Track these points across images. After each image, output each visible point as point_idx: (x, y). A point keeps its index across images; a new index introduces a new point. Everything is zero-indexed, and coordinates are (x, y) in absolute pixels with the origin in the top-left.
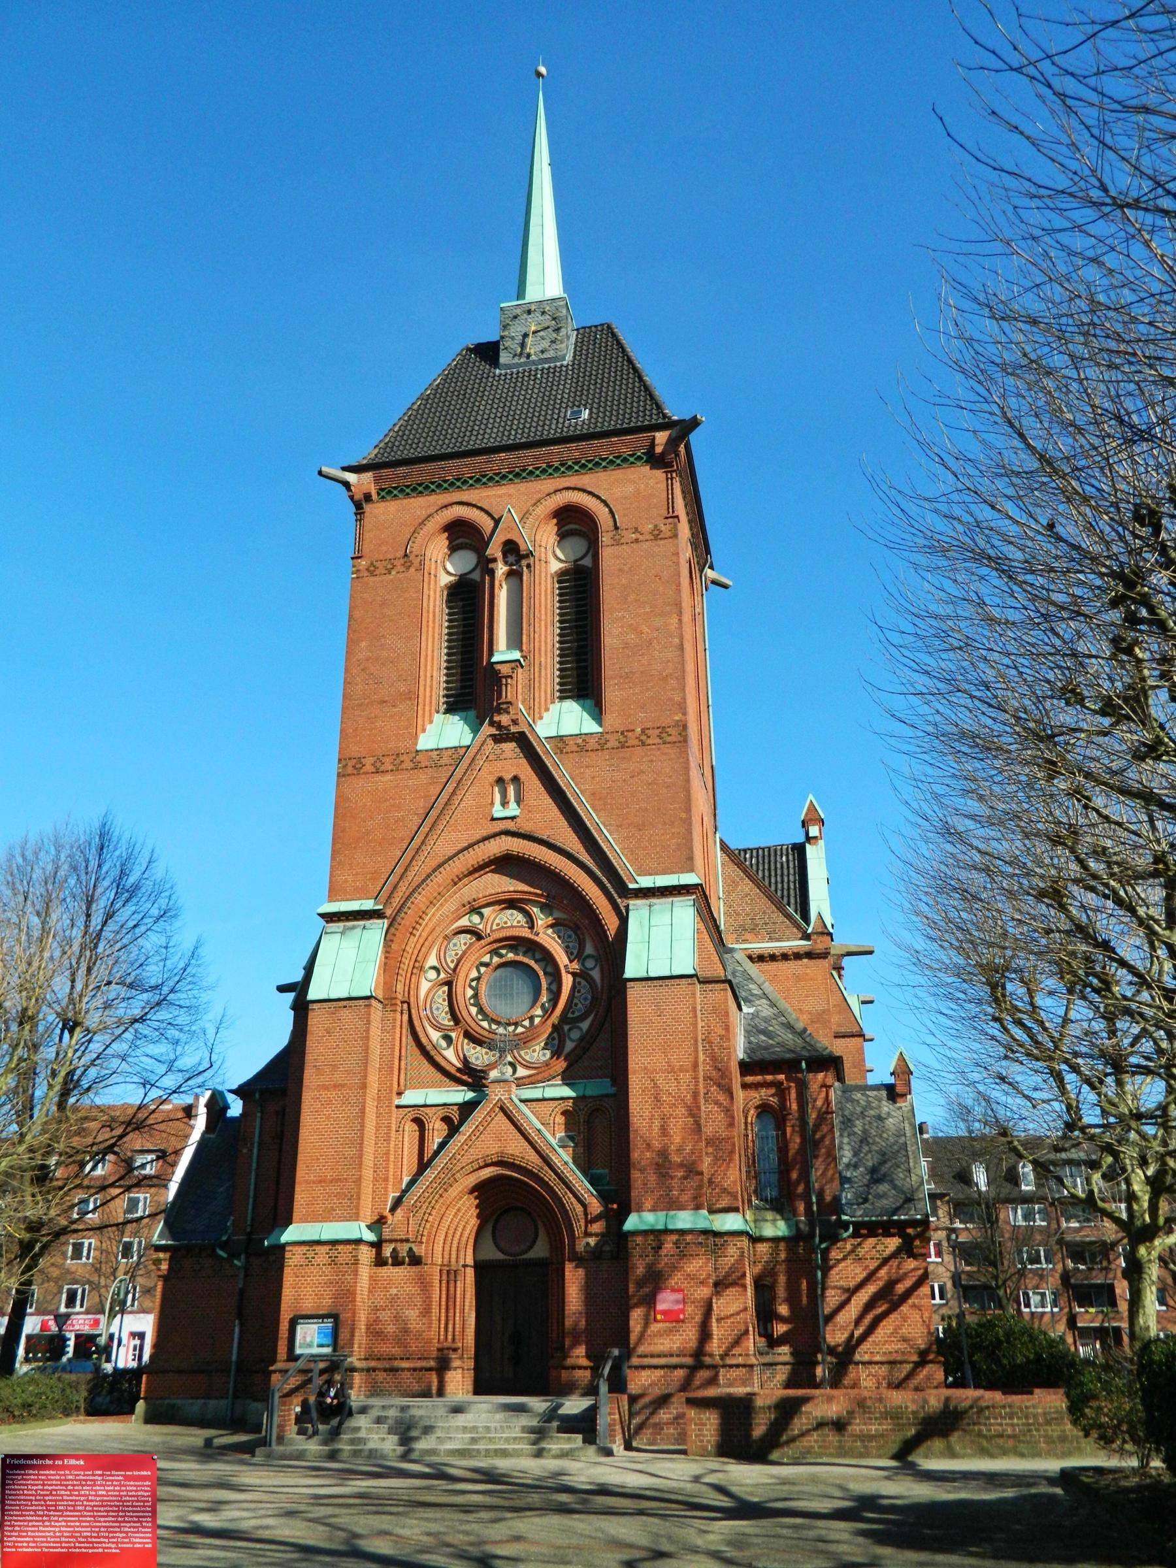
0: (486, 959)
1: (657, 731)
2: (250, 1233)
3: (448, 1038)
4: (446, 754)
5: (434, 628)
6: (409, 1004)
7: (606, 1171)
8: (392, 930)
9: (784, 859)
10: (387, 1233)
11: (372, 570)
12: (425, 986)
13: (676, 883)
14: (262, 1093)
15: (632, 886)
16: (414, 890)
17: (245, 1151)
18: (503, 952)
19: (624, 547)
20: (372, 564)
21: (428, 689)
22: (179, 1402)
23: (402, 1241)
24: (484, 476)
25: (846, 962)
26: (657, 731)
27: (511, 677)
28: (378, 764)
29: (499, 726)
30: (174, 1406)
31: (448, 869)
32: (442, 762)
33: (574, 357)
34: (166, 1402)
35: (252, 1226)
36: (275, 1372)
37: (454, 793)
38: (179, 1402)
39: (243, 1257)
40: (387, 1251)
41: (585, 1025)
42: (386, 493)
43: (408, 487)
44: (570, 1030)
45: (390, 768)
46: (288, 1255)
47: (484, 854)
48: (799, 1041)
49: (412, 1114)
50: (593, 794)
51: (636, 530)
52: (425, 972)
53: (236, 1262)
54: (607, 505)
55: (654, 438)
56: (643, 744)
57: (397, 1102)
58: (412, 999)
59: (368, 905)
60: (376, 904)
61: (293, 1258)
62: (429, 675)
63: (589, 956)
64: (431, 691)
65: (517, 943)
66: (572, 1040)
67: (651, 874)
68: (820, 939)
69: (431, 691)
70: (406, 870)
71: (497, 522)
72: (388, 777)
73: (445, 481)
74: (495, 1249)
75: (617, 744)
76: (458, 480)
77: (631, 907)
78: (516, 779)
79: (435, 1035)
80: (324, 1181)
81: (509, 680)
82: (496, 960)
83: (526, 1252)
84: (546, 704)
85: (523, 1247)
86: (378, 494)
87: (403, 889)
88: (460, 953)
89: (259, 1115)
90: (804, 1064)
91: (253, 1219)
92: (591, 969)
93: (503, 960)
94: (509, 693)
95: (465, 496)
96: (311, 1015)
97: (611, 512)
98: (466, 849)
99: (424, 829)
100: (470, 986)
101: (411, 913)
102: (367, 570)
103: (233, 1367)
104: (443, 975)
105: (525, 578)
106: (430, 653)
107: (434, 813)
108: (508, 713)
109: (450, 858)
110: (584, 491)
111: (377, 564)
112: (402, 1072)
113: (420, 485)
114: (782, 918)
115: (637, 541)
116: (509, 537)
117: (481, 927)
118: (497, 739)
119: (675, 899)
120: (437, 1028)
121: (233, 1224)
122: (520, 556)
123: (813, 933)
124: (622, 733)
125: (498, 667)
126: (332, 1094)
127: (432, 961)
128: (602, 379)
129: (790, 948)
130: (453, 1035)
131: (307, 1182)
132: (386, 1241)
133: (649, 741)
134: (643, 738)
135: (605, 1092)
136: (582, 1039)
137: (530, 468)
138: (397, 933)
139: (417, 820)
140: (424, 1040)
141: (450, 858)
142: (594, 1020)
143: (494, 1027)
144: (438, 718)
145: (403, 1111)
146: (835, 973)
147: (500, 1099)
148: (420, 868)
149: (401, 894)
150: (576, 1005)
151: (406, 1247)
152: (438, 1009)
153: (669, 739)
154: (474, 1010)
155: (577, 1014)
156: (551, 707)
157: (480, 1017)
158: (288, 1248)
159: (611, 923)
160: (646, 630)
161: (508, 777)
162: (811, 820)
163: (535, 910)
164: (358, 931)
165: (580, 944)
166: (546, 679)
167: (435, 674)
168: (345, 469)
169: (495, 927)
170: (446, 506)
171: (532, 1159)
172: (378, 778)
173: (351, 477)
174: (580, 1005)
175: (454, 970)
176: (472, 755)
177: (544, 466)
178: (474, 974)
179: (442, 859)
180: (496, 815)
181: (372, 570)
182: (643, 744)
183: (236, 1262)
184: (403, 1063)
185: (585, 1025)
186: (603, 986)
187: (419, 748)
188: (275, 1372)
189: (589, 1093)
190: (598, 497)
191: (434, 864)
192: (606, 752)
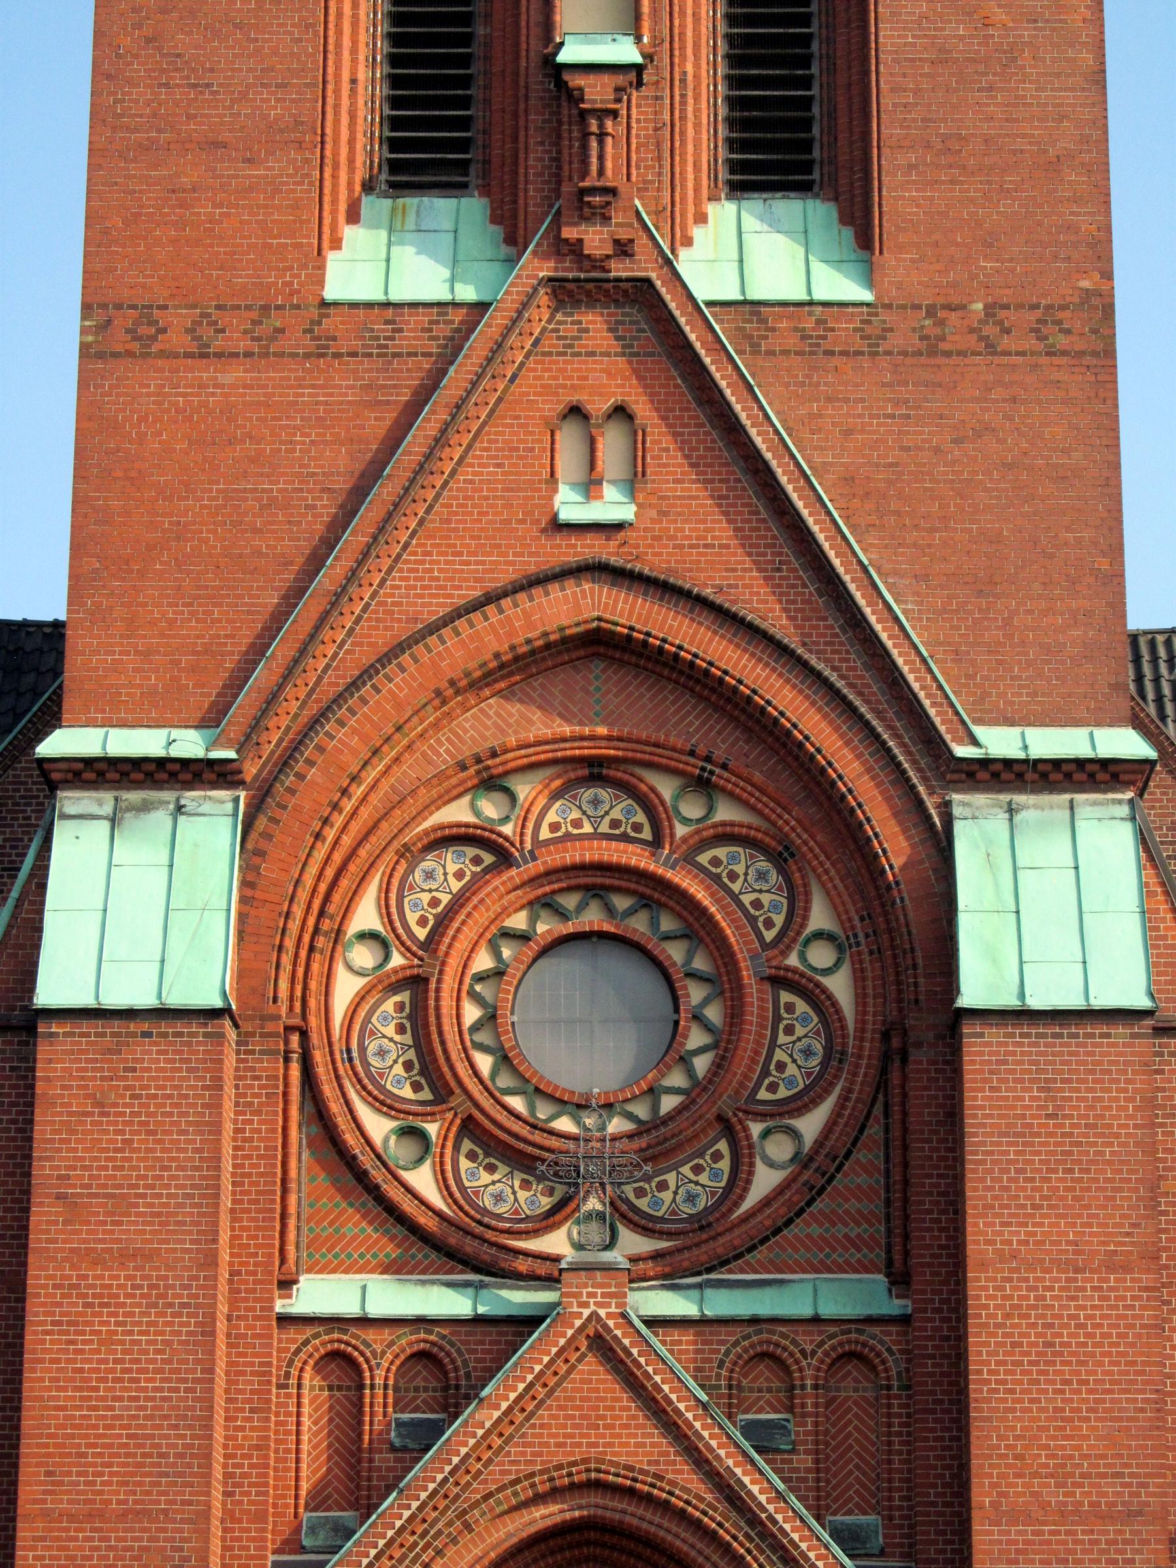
0: (519, 921)
1: (1032, 317)
6: (304, 1034)
7: (871, 1518)
8: (261, 823)
12: (346, 988)
15: (962, 751)
18: (570, 901)
26: (1032, 317)
27: (615, 114)
28: (206, 332)
29: (575, 249)
31: (425, 658)
32: (402, 343)
37: (441, 440)
41: (810, 1125)
44: (766, 1134)
45: (242, 346)
47: (530, 626)
49: (323, 1341)
52: (348, 946)
56: (991, 348)
57: (280, 1306)
58: (314, 1022)
60: (213, 744)
62: (346, 76)
63: (819, 935)
66: (771, 1164)
67: (1010, 722)
72: (232, 375)
77: (957, 811)
78: (621, 412)
80: (101, 1515)
81: (609, 124)
82: (544, 927)
84: (697, 203)
88: (445, 899)
92: (827, 972)
93: (569, 928)
96: (43, 1050)
98: (476, 606)
99: (354, 538)
100: (473, 995)
104: (397, 960)
107: (384, 492)
108: (606, 219)
109: (433, 629)
112: (292, 1222)
117: (507, 829)
119: (1080, 797)
120: (386, 1105)
124: (931, 312)
125: (576, 81)
130: (432, 1129)
131: (46, 1514)
133: (1005, 342)
134: (990, 330)
135: (874, 1311)
136: (801, 1161)
138: (276, 831)
139: (327, 508)
140: (351, 1139)
141: (433, 629)
142: (836, 1114)
143: (543, 1111)
144: (723, 213)
145: (298, 1335)
147: (594, 1315)
149: (285, 722)
152: (382, 1053)
153: (1062, 341)
154: (485, 1063)
156: (711, 209)
160: (1000, 15)
163: (666, 788)
164: (160, 819)
166: (698, 126)
167: (361, 76)
169: (545, 834)
172: (207, 373)
176: (494, 332)
178: (483, 962)
179: (401, 631)
182: (991, 348)
184: (293, 1199)
185: (810, 1125)
186: (861, 1022)
187: (331, 293)
189: (828, 1309)
191: (382, 640)
192: (884, 362)
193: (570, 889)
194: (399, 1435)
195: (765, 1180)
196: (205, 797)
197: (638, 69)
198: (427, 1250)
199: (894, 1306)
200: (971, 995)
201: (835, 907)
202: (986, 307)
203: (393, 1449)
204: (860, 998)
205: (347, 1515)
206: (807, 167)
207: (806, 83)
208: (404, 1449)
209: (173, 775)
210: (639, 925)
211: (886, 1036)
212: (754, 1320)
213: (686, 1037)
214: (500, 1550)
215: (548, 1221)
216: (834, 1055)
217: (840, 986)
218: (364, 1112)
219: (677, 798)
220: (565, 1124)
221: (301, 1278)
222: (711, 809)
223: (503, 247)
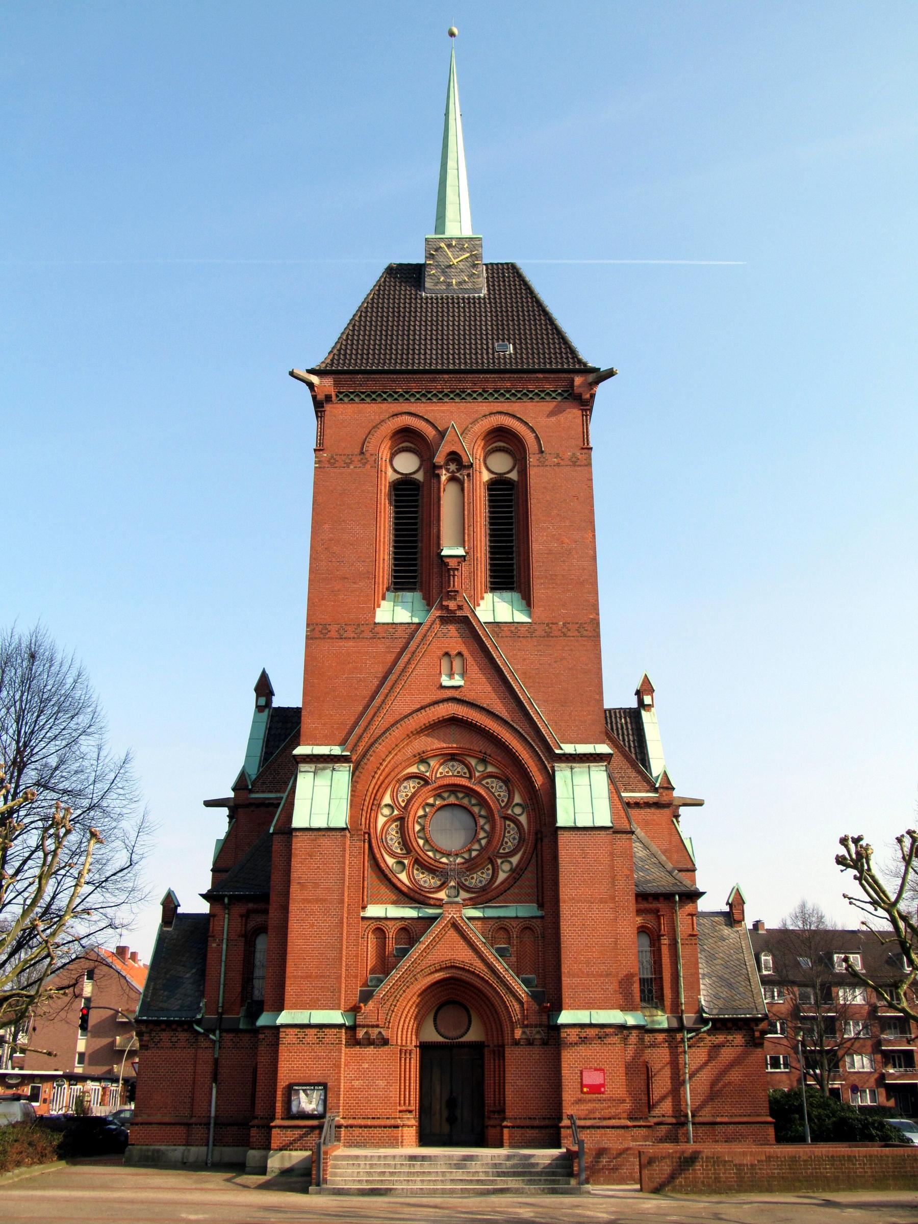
0: (431, 801)
2: (222, 1014)
3: (400, 863)
4: (400, 628)
5: (385, 518)
6: (369, 835)
8: (357, 773)
9: (623, 720)
10: (360, 1020)
11: (332, 462)
12: (381, 820)
13: (593, 751)
14: (230, 897)
16: (375, 741)
17: (214, 945)
19: (547, 468)
20: (332, 457)
21: (381, 570)
22: (163, 1148)
23: (373, 1026)
24: (430, 392)
25: (682, 810)
27: (457, 569)
28: (342, 632)
30: (158, 1151)
32: (397, 635)
33: (489, 290)
34: (152, 1147)
35: (222, 1007)
36: (275, 1127)
37: (408, 663)
38: (163, 1148)
39: (218, 1032)
40: (361, 1033)
41: (515, 860)
42: (343, 396)
43: (363, 393)
44: (502, 863)
45: (352, 635)
46: (282, 1035)
47: (434, 716)
48: (670, 879)
49: (374, 925)
50: (525, 673)
51: (557, 456)
52: (382, 809)
53: (212, 1036)
54: (533, 430)
55: (573, 381)
57: (362, 914)
58: (372, 831)
59: (337, 750)
61: (287, 1038)
62: (382, 558)
63: (517, 804)
64: (383, 571)
65: (453, 789)
66: (504, 871)
68: (665, 792)
69: (383, 571)
70: (369, 723)
71: (442, 434)
73: (396, 393)
74: (436, 1033)
75: (543, 634)
76: (407, 393)
78: (460, 654)
79: (390, 861)
80: (310, 977)
83: (462, 1036)
84: (481, 593)
85: (459, 1033)
86: (337, 396)
87: (366, 740)
88: (410, 794)
89: (227, 916)
90: (677, 897)
91: (223, 1003)
92: (519, 815)
93: (445, 803)
94: (456, 583)
95: (413, 408)
96: (294, 840)
97: (537, 437)
99: (384, 690)
101: (372, 759)
102: (329, 461)
103: (212, 1121)
104: (396, 812)
105: (466, 485)
106: (382, 540)
107: (392, 677)
108: (455, 599)
109: (406, 717)
110: (514, 416)
111: (337, 458)
113: (374, 393)
114: (634, 774)
115: (558, 464)
116: (453, 448)
117: (427, 774)
118: (444, 620)
120: (393, 855)
121: (206, 1005)
122: (461, 466)
123: (659, 787)
124: (548, 625)
126: (316, 907)
127: (387, 800)
128: (518, 316)
129: (642, 798)
130: (406, 862)
131: (295, 977)
132: (360, 1026)
135: (534, 915)
136: (512, 871)
137: (469, 391)
138: (362, 776)
140: (382, 865)
141: (406, 717)
146: (674, 820)
148: (380, 723)
149: (364, 744)
150: (506, 843)
151: (376, 1030)
152: (392, 839)
153: (585, 633)
154: (421, 842)
155: (507, 850)
156: (485, 595)
157: (427, 847)
158: (281, 1030)
159: (538, 780)
161: (453, 653)
162: (645, 690)
163: (473, 762)
164: (328, 772)
165: (509, 794)
166: (481, 572)
168: (312, 372)
169: (438, 775)
170: (396, 415)
171: (479, 966)
172: (342, 643)
173: (315, 379)
174: (509, 844)
175: (405, 807)
177: (480, 391)
180: (444, 684)
181: (332, 462)
182: (565, 635)
183: (212, 1036)
185: (515, 860)
187: (377, 620)
188: (253, 1126)
190: (526, 424)
193: (462, 792)
201: (522, 797)
205: (381, 976)
206: (512, 583)
208: (398, 956)
209: (318, 759)
210: (465, 802)
211: (536, 834)
216: (522, 840)
217: (523, 819)
219: (476, 765)
220: (444, 860)
222: (486, 768)
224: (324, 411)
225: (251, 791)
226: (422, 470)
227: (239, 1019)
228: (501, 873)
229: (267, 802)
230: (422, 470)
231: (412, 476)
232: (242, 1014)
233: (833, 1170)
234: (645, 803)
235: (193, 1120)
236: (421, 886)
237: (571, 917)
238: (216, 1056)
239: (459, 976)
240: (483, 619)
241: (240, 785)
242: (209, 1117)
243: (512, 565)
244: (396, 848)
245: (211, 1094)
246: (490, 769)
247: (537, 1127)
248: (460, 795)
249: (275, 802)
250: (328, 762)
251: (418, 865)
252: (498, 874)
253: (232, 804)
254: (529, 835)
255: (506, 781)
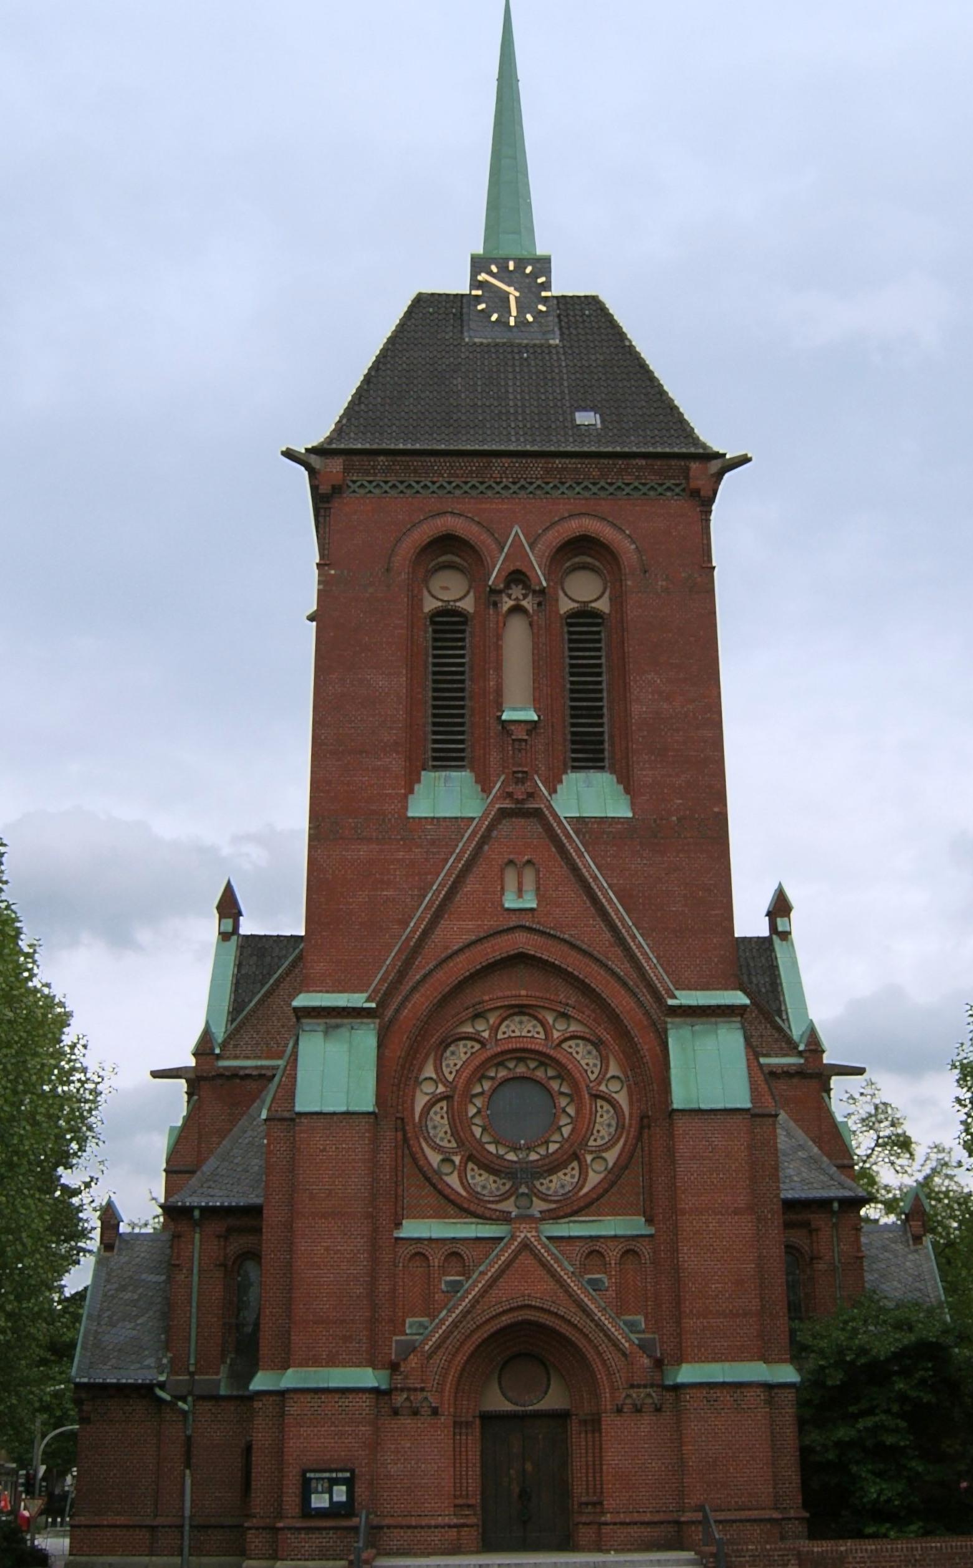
15: (670, 1002)
25: (835, 1081)
35: (196, 1364)
39: (190, 1399)
44: (593, 1160)
59: (358, 1000)
103: (187, 1522)
120: (437, 1148)
129: (782, 1066)
137: (539, 482)
151: (420, 1396)
173: (314, 460)
185: (611, 1156)
188: (250, 1528)
193: (512, 1059)
194: (446, 1286)
195: (593, 1179)
196: (362, 1023)
197: (535, 722)
198: (456, 1209)
199: (651, 1230)
200: (679, 1101)
201: (621, 1066)
202: (678, 819)
203: (443, 1292)
204: (631, 1103)
205: (425, 1319)
206: (602, 760)
207: (601, 725)
208: (448, 1292)
209: (339, 1013)
210: (521, 1070)
211: (642, 1119)
212: (591, 1237)
213: (559, 1120)
214: (489, 1333)
215: (504, 1197)
216: (620, 1126)
217: (622, 1099)
218: (428, 1151)
219: (554, 1021)
220: (511, 1157)
221: (404, 1222)
222: (569, 1026)
223: (481, 793)
224: (330, 508)
225: (219, 1057)
226: (471, 594)
227: (220, 1381)
228: (591, 1174)
229: (242, 1073)
230: (471, 594)
231: (458, 604)
232: (224, 1370)
233: (429, 1539)
234: (784, 1072)
235: (159, 1521)
236: (478, 1193)
237: (694, 1234)
238: (189, 1432)
239: (536, 1319)
240: (563, 813)
241: (204, 1049)
242: (183, 1516)
243: (602, 734)
244: (442, 1139)
245: (183, 1485)
246: (574, 1028)
247: (648, 1524)
248: (511, 1065)
249: (269, 1073)
250: (346, 1017)
251: (474, 1163)
252: (587, 1176)
253: (192, 1075)
254: (630, 1119)
255: (597, 1044)
